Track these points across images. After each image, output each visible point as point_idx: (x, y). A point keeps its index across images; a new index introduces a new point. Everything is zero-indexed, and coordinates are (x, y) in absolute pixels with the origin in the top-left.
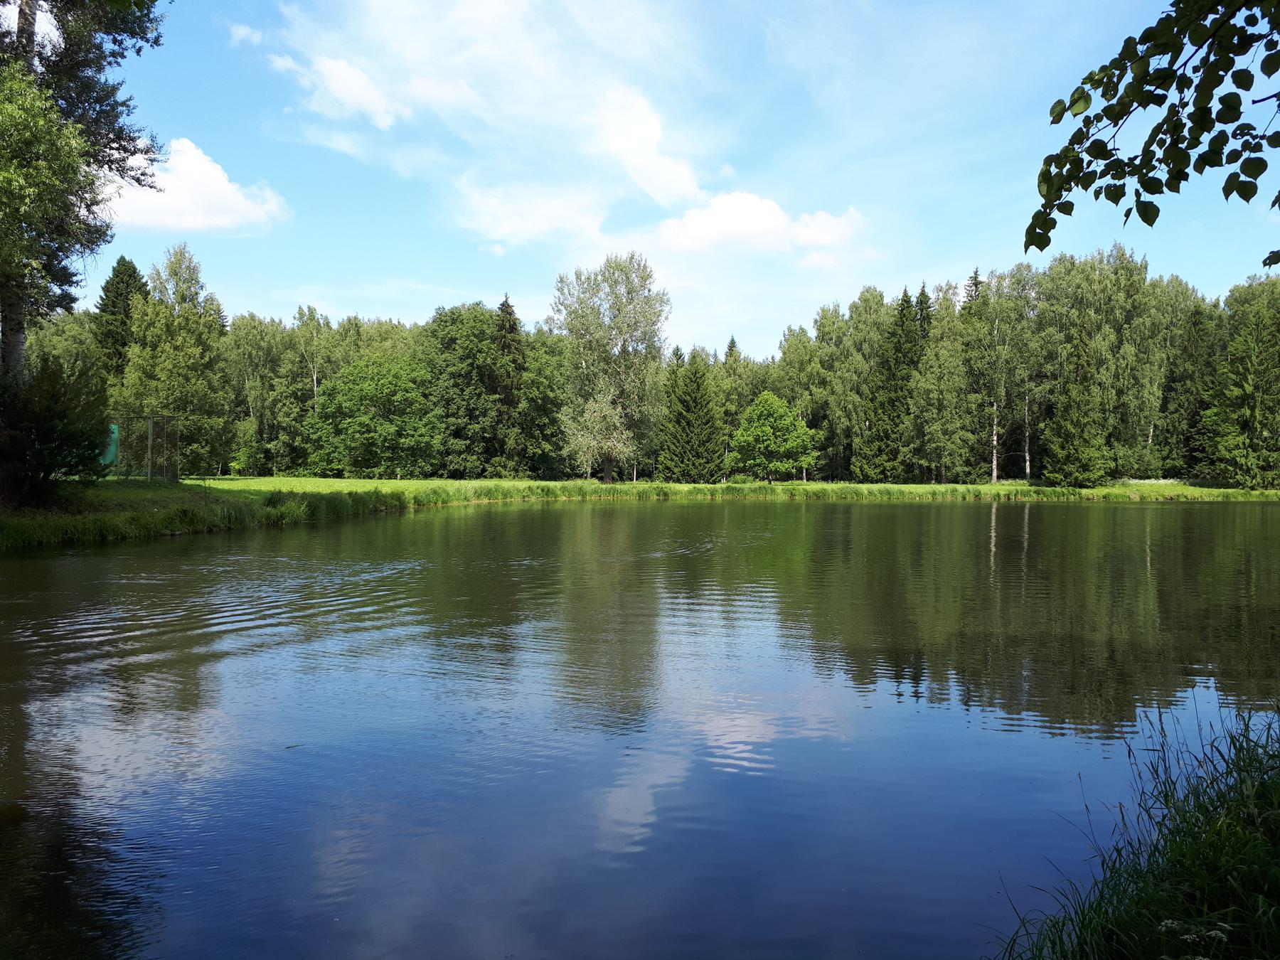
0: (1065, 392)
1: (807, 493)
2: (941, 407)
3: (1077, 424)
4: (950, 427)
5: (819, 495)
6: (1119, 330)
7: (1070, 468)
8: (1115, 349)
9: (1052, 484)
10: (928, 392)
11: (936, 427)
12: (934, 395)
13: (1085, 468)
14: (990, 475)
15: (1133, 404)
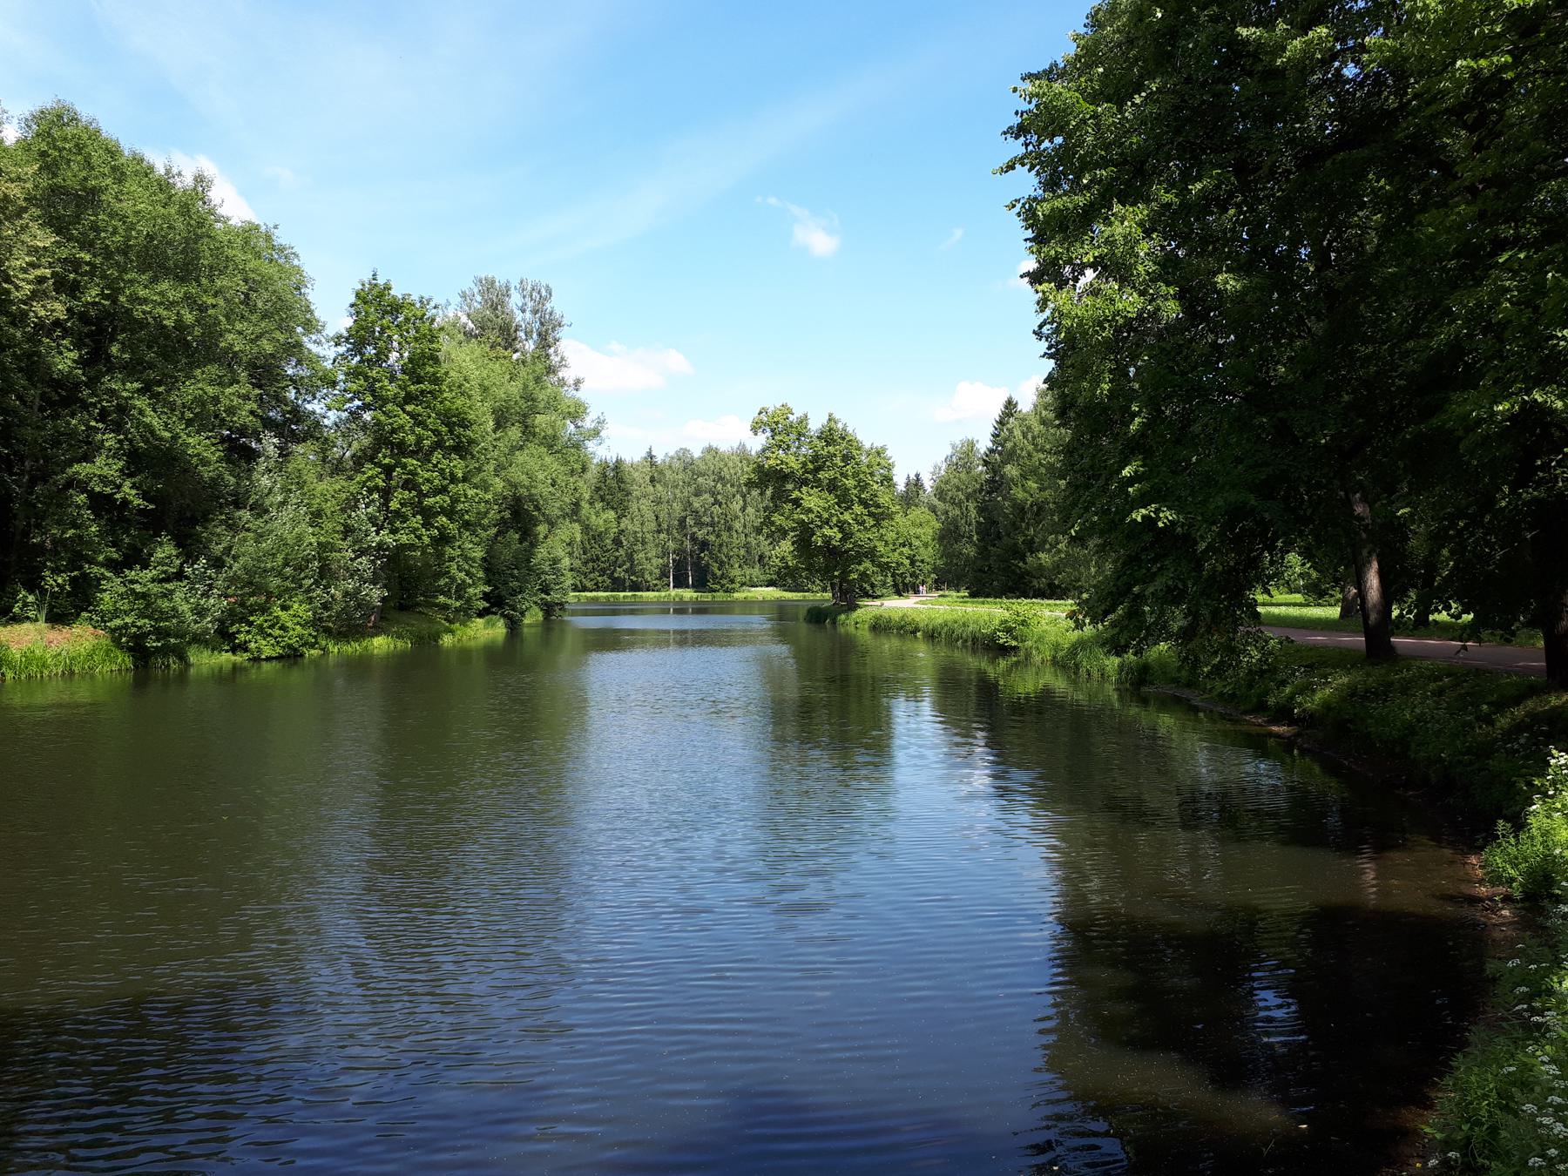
0: (718, 536)
6: (744, 496)
8: (743, 509)
11: (642, 555)
13: (732, 581)
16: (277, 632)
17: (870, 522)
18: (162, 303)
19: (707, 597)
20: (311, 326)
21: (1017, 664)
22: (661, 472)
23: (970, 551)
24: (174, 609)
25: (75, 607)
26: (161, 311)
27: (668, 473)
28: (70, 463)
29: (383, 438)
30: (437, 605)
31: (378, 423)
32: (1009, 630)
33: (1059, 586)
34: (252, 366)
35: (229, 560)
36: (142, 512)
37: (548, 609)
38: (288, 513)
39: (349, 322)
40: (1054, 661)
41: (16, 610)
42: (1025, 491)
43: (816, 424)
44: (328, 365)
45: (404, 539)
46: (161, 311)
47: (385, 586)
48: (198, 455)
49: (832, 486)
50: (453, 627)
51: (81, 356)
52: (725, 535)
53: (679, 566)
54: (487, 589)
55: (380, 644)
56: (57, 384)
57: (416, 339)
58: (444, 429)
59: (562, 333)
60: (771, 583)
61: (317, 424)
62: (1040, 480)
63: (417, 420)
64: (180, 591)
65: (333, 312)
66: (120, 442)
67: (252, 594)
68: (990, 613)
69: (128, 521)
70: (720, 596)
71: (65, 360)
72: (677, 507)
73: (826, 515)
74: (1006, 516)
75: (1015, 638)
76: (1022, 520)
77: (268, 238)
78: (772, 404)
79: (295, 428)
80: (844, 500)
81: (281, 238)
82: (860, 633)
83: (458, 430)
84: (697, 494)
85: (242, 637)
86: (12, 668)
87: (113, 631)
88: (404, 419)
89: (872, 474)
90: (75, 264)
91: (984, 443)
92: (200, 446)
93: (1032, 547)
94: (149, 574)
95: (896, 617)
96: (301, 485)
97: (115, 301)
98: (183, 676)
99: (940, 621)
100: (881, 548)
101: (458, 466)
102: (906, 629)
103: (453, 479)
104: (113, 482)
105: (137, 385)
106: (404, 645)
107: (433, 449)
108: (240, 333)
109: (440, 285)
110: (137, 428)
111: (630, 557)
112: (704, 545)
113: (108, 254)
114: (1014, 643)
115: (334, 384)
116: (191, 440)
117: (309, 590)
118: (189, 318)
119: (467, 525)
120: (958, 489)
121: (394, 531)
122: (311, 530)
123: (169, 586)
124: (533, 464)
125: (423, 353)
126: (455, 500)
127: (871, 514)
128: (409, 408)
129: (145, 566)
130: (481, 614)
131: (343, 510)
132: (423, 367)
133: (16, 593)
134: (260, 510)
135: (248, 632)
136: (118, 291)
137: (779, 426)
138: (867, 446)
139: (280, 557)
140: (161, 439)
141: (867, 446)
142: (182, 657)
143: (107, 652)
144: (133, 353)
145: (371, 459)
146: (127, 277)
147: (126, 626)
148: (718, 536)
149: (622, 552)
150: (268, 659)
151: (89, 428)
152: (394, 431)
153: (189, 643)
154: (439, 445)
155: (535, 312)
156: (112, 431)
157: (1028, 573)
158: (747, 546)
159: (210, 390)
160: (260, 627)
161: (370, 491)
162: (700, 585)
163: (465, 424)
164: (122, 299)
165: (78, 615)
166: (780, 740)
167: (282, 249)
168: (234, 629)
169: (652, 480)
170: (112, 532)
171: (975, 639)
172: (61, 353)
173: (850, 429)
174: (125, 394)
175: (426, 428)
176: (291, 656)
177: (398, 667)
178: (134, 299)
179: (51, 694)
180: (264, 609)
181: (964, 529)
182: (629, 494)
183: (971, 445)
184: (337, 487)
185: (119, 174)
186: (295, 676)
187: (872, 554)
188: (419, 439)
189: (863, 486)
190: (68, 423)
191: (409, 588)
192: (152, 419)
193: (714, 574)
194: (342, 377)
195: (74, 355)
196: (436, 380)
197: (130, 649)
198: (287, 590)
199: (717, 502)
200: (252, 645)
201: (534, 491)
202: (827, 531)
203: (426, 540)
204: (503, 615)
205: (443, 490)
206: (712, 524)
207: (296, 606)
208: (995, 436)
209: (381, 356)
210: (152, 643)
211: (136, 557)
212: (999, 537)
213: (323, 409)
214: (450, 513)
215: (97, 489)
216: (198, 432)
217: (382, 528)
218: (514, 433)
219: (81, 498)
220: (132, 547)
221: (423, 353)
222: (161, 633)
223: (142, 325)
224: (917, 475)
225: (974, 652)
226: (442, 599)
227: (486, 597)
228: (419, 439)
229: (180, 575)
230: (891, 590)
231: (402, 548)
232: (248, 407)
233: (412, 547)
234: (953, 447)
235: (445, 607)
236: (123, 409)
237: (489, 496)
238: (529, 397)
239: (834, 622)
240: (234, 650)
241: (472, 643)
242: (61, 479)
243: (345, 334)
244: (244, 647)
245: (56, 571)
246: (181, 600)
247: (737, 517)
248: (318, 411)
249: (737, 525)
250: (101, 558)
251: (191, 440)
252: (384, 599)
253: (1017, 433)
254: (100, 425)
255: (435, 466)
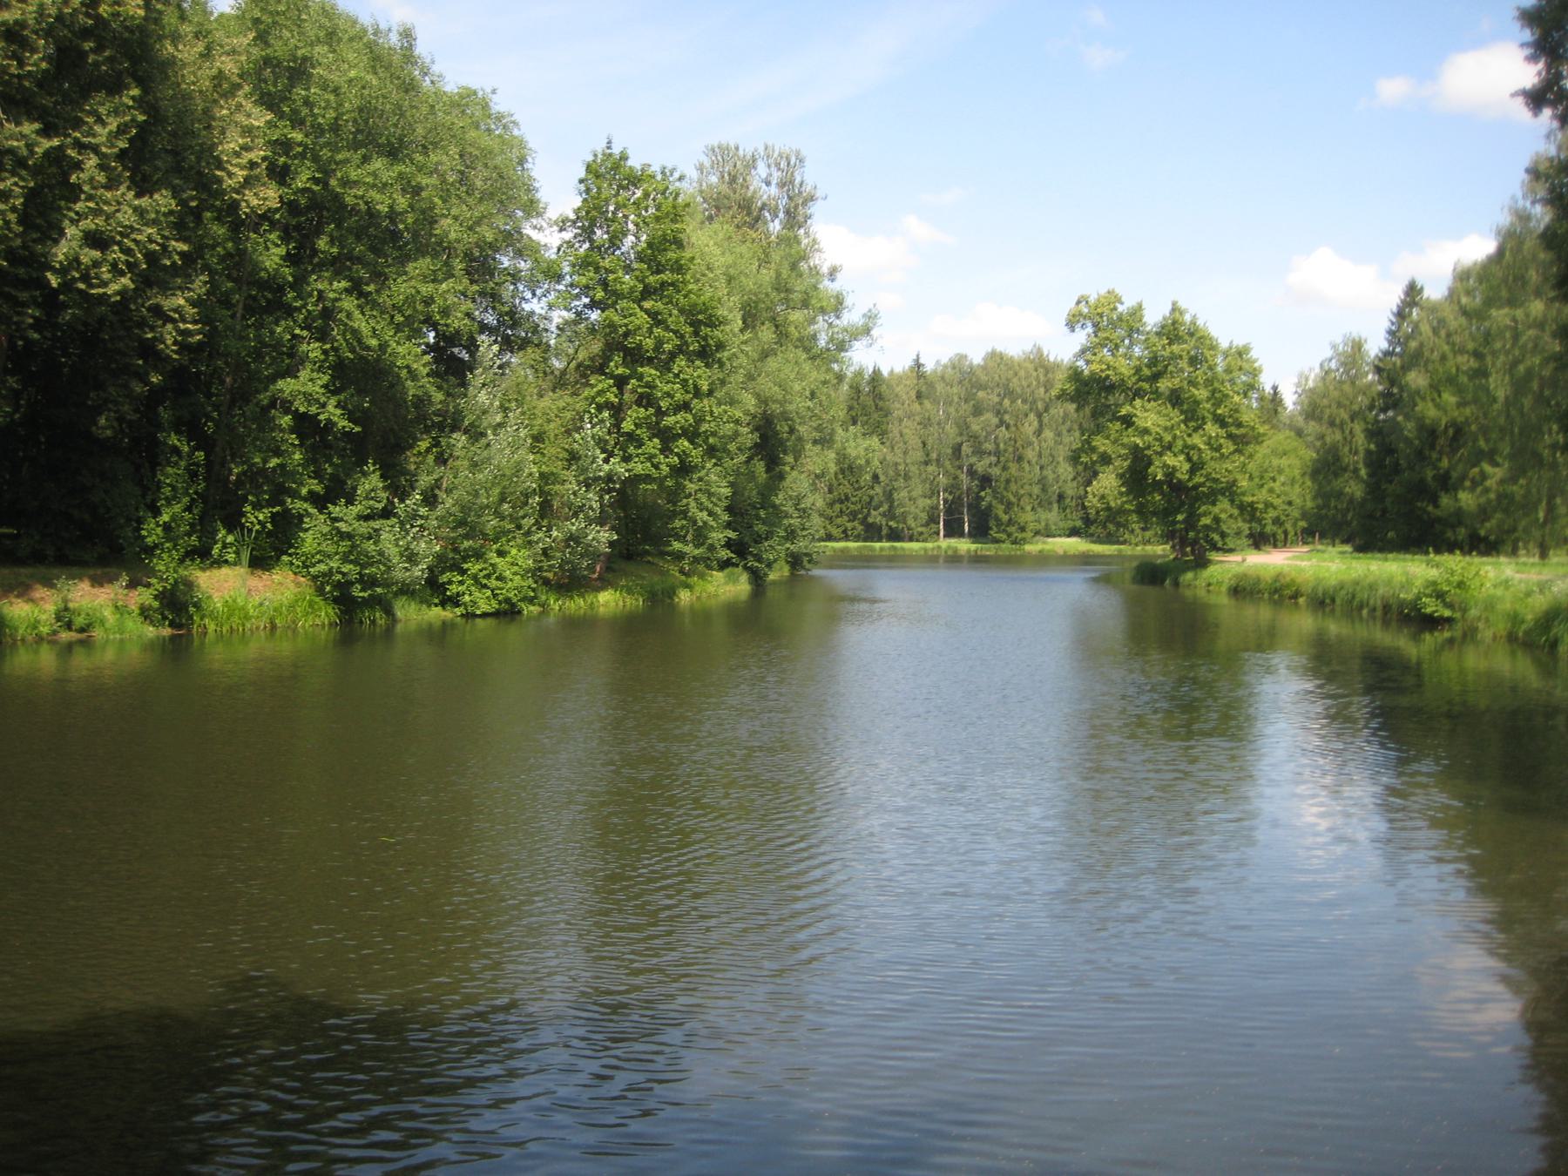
0: (1005, 468)
1: (834, 550)
2: (907, 477)
3: (1016, 494)
4: (914, 494)
5: (843, 550)
6: (1039, 416)
7: (1011, 529)
8: (1039, 432)
9: (997, 541)
10: (896, 464)
11: (904, 494)
12: (901, 467)
13: (1023, 529)
14: (938, 534)
15: (1051, 476)
16: (493, 583)
17: (1228, 447)
18: (374, 186)
19: (988, 549)
20: (532, 208)
21: (1451, 641)
22: (931, 385)
23: (1355, 489)
24: (381, 553)
25: (275, 549)
26: (373, 194)
27: (940, 387)
28: (273, 379)
29: (618, 345)
30: (669, 554)
31: (612, 326)
32: (1440, 596)
33: (1485, 539)
34: (468, 256)
35: (442, 495)
36: (348, 435)
37: (795, 561)
38: (506, 435)
39: (577, 202)
40: (1511, 638)
41: (215, 551)
42: (1438, 406)
43: (1153, 317)
44: (551, 254)
45: (639, 468)
46: (373, 194)
47: (613, 528)
48: (408, 367)
49: (1175, 399)
50: (690, 580)
51: (288, 253)
52: (1013, 468)
53: (952, 509)
54: (732, 535)
55: (607, 600)
56: (263, 285)
57: (657, 219)
58: (689, 329)
59: (815, 209)
60: (1074, 532)
61: (535, 329)
62: (1460, 390)
63: (656, 319)
64: (388, 533)
65: (558, 191)
66: (325, 352)
67: (467, 537)
68: (1406, 573)
69: (329, 446)
70: (1006, 548)
71: (272, 256)
72: (951, 429)
73: (1168, 438)
74: (1408, 441)
75: (1450, 606)
76: (1432, 447)
77: (485, 106)
78: (1094, 292)
79: (516, 333)
80: (1192, 417)
81: (499, 105)
82: (1213, 599)
83: (704, 330)
84: (977, 411)
85: (454, 589)
86: (214, 618)
87: (315, 578)
88: (642, 319)
89: (1232, 381)
90: (284, 145)
91: (1376, 344)
92: (411, 356)
93: (1446, 483)
94: (355, 510)
95: (1268, 576)
96: (520, 403)
97: (326, 184)
98: (389, 631)
99: (1333, 582)
100: (1244, 483)
101: (701, 375)
102: (1282, 593)
103: (697, 393)
104: (317, 401)
105: (344, 284)
106: (635, 603)
107: (673, 356)
108: (456, 218)
109: (674, 150)
110: (344, 335)
111: (889, 496)
112: (986, 480)
113: (319, 130)
114: (1447, 613)
115: (559, 278)
116: (400, 349)
117: (528, 533)
118: (402, 202)
119: (711, 451)
120: (1339, 405)
121: (626, 459)
122: (532, 457)
123: (376, 524)
124: (789, 372)
125: (664, 235)
126: (699, 420)
127: (1230, 436)
128: (647, 305)
129: (350, 502)
130: (724, 565)
131: (568, 432)
132: (663, 253)
133: (216, 531)
134: (475, 434)
135: (461, 583)
136: (328, 173)
137: (1105, 320)
138: (1224, 344)
139: (497, 491)
140: (368, 348)
141: (1224, 344)
142: (389, 612)
143: (311, 603)
144: (342, 247)
145: (601, 370)
146: (339, 157)
147: (331, 572)
148: (1005, 468)
149: (878, 489)
150: (485, 615)
151: (294, 336)
152: (626, 335)
153: (396, 595)
154: (681, 350)
155: (782, 185)
156: (317, 340)
157: (1439, 520)
158: (1042, 482)
159: (427, 289)
160: (475, 578)
161: (600, 408)
162: (980, 532)
163: (713, 322)
164: (333, 182)
165: (278, 559)
166: (1137, 726)
167: (499, 118)
168: (444, 578)
169: (919, 396)
170: (314, 461)
171: (1387, 608)
172: (267, 249)
173: (1200, 322)
174: (332, 295)
175: (667, 329)
176: (508, 612)
177: (627, 628)
178: (346, 183)
179: (255, 648)
180: (479, 555)
181: (1348, 459)
182: (887, 414)
183: (1357, 346)
184: (561, 404)
185: (331, 37)
186: (513, 634)
187: (1230, 491)
188: (659, 343)
189: (1218, 398)
190: (272, 332)
191: (642, 530)
192: (361, 323)
193: (997, 519)
194: (567, 269)
195: (282, 251)
196: (679, 268)
197: (336, 601)
198: (506, 533)
199: (1002, 422)
200: (467, 598)
201: (790, 407)
202: (1169, 460)
203: (665, 469)
204: (746, 568)
205: (686, 406)
206: (998, 453)
207: (514, 551)
208: (1391, 332)
209: (615, 241)
210: (357, 592)
211: (336, 492)
212: (1396, 469)
213: (545, 308)
214: (692, 435)
215: (302, 409)
216: (409, 339)
217: (611, 455)
218: (767, 334)
219: (286, 421)
220: (334, 477)
221: (664, 235)
222: (369, 582)
223: (354, 211)
224: (1275, 388)
225: (1386, 623)
226: (677, 545)
227: (729, 544)
228: (659, 343)
229: (387, 513)
230: (1245, 542)
231: (635, 480)
232: (463, 308)
233: (647, 478)
234: (1334, 347)
235: (679, 556)
236: (328, 314)
237: (738, 414)
238: (782, 287)
239: (1176, 584)
240: (443, 604)
241: (713, 602)
242: (264, 398)
243: (572, 216)
244: (454, 601)
245: (257, 506)
246: (389, 539)
247: (1030, 444)
248: (538, 311)
249: (1030, 454)
250: (304, 491)
251: (400, 349)
252: (611, 544)
253: (1425, 329)
254: (305, 333)
255: (677, 376)
